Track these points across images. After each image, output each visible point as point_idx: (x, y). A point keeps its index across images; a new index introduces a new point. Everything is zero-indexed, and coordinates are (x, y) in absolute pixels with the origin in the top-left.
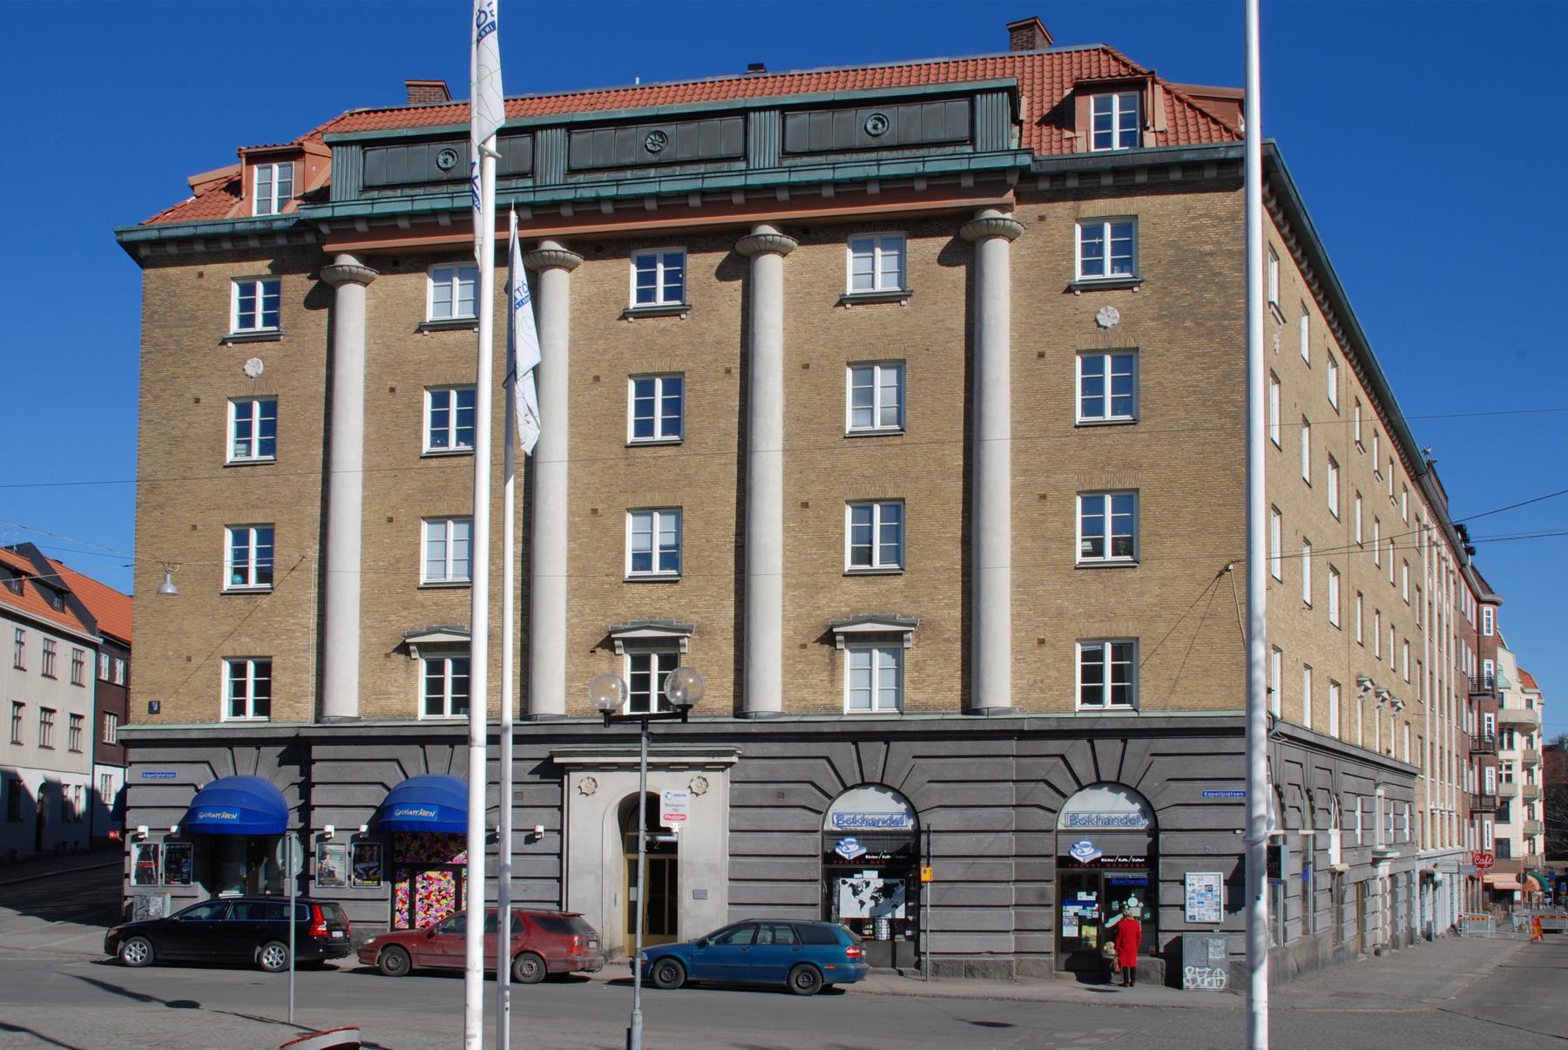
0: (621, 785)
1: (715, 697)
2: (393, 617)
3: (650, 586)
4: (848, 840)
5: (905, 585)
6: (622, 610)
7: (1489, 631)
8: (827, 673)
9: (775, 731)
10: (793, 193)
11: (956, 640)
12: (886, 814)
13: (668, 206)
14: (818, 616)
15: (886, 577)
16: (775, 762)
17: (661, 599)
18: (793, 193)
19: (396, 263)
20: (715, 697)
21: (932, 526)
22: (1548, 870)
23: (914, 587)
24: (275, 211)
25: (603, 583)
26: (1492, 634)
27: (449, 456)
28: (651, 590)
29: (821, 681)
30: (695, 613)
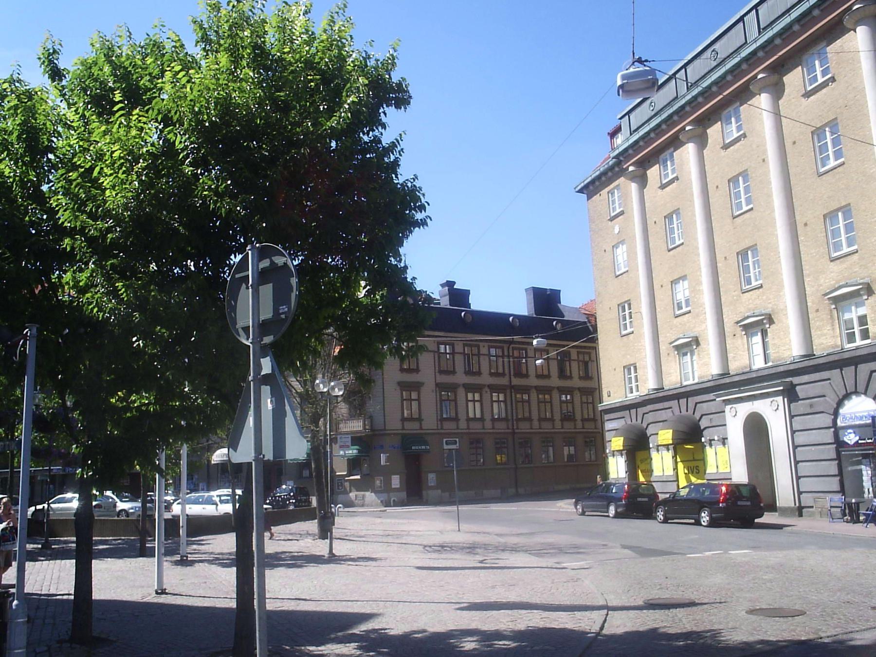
0: (744, 409)
1: (784, 350)
2: (668, 335)
3: (751, 293)
4: (849, 431)
5: (859, 259)
6: (743, 310)
7: (455, 443)
8: (830, 325)
9: (800, 366)
10: (821, 8)
11: (65, 564)
12: (864, 412)
13: (826, 8)
14: (821, 290)
15: (849, 257)
16: (806, 386)
17: (755, 299)
18: (821, 8)
19: (783, 66)
20: (784, 350)
21: (866, 216)
22: (735, 489)
23: (864, 258)
24: (184, 451)
25: (733, 296)
26: (446, 447)
27: (832, 170)
28: (751, 295)
29: (829, 330)
30: (770, 303)
